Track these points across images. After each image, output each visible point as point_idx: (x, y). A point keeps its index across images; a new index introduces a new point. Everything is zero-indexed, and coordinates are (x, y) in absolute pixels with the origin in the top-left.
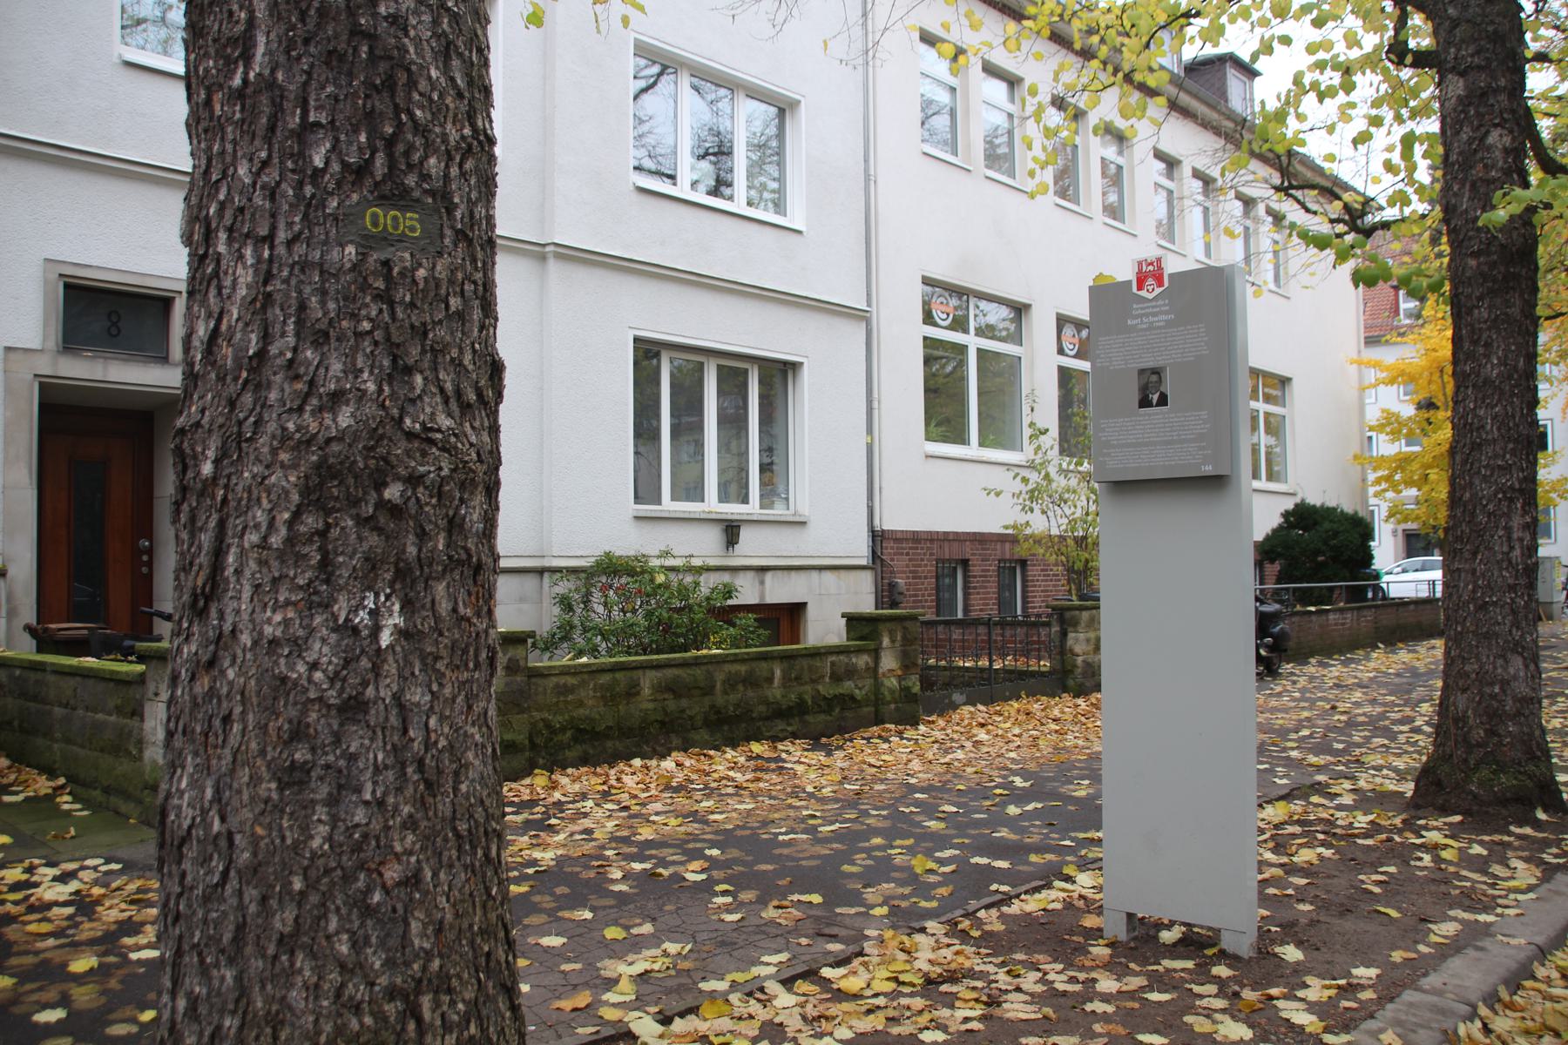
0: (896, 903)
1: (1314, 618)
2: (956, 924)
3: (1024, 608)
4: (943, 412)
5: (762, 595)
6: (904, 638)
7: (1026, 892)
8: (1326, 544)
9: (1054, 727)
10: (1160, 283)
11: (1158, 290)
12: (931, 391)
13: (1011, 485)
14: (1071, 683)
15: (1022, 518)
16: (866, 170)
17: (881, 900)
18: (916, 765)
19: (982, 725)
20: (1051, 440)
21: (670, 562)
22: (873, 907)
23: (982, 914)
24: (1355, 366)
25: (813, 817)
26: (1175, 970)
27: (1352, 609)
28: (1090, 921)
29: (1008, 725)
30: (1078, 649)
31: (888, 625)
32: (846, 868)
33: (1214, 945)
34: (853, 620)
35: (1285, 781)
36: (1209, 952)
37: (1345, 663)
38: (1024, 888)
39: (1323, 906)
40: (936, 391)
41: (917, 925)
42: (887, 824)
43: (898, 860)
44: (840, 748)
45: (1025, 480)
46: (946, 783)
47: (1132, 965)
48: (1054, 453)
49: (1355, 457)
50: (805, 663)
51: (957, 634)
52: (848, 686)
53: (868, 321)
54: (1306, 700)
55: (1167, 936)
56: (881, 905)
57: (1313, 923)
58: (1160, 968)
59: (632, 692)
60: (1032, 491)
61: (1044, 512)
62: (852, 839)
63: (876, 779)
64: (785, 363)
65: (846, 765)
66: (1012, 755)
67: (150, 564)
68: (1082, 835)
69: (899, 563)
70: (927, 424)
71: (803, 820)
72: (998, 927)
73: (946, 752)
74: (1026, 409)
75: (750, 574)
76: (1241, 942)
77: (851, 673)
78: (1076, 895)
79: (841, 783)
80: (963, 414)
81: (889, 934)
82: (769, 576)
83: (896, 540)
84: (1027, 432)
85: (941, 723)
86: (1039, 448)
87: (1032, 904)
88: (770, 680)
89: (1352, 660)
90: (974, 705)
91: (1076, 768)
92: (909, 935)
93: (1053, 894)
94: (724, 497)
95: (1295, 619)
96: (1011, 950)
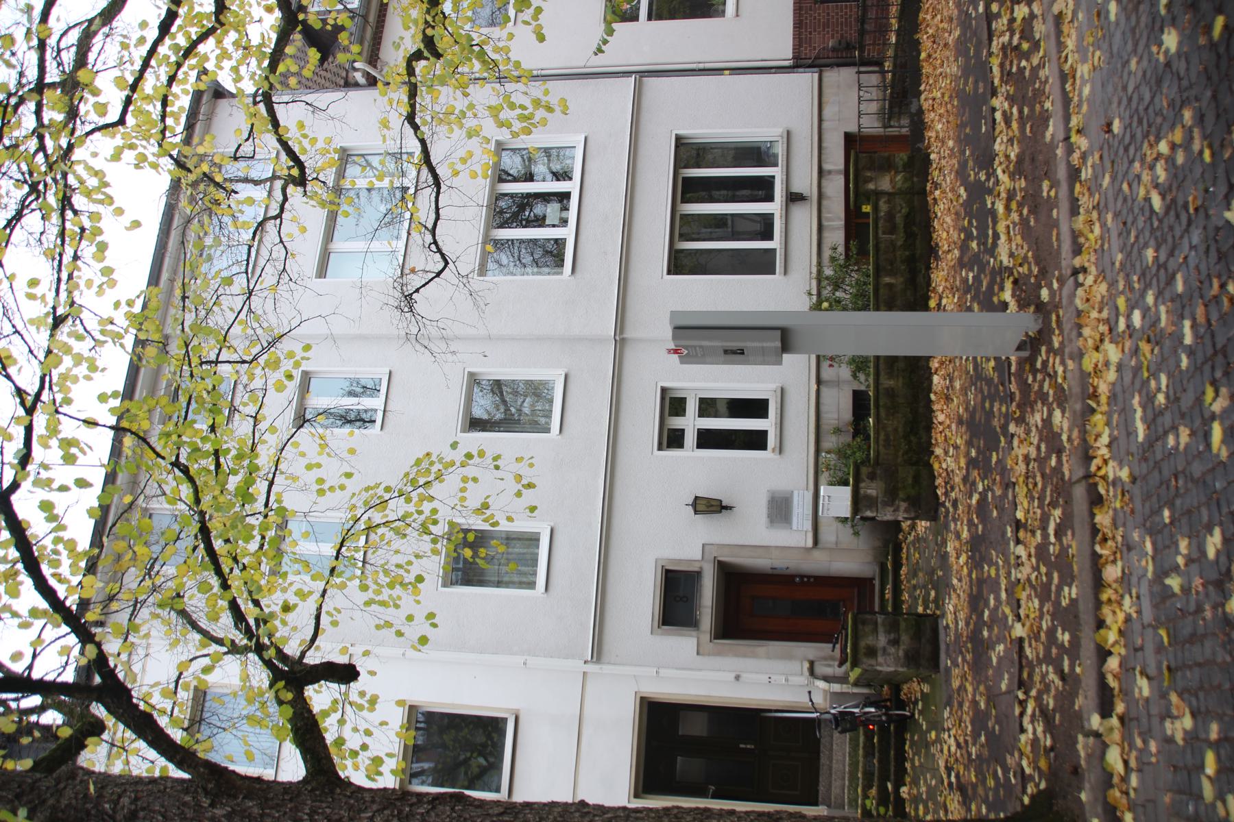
5: (838, 172)
21: (814, 292)
52: (899, 219)
59: (891, 393)
64: (677, 147)
67: (809, 577)
75: (824, 182)
82: (826, 167)
83: (800, 46)
88: (890, 286)
94: (769, 198)
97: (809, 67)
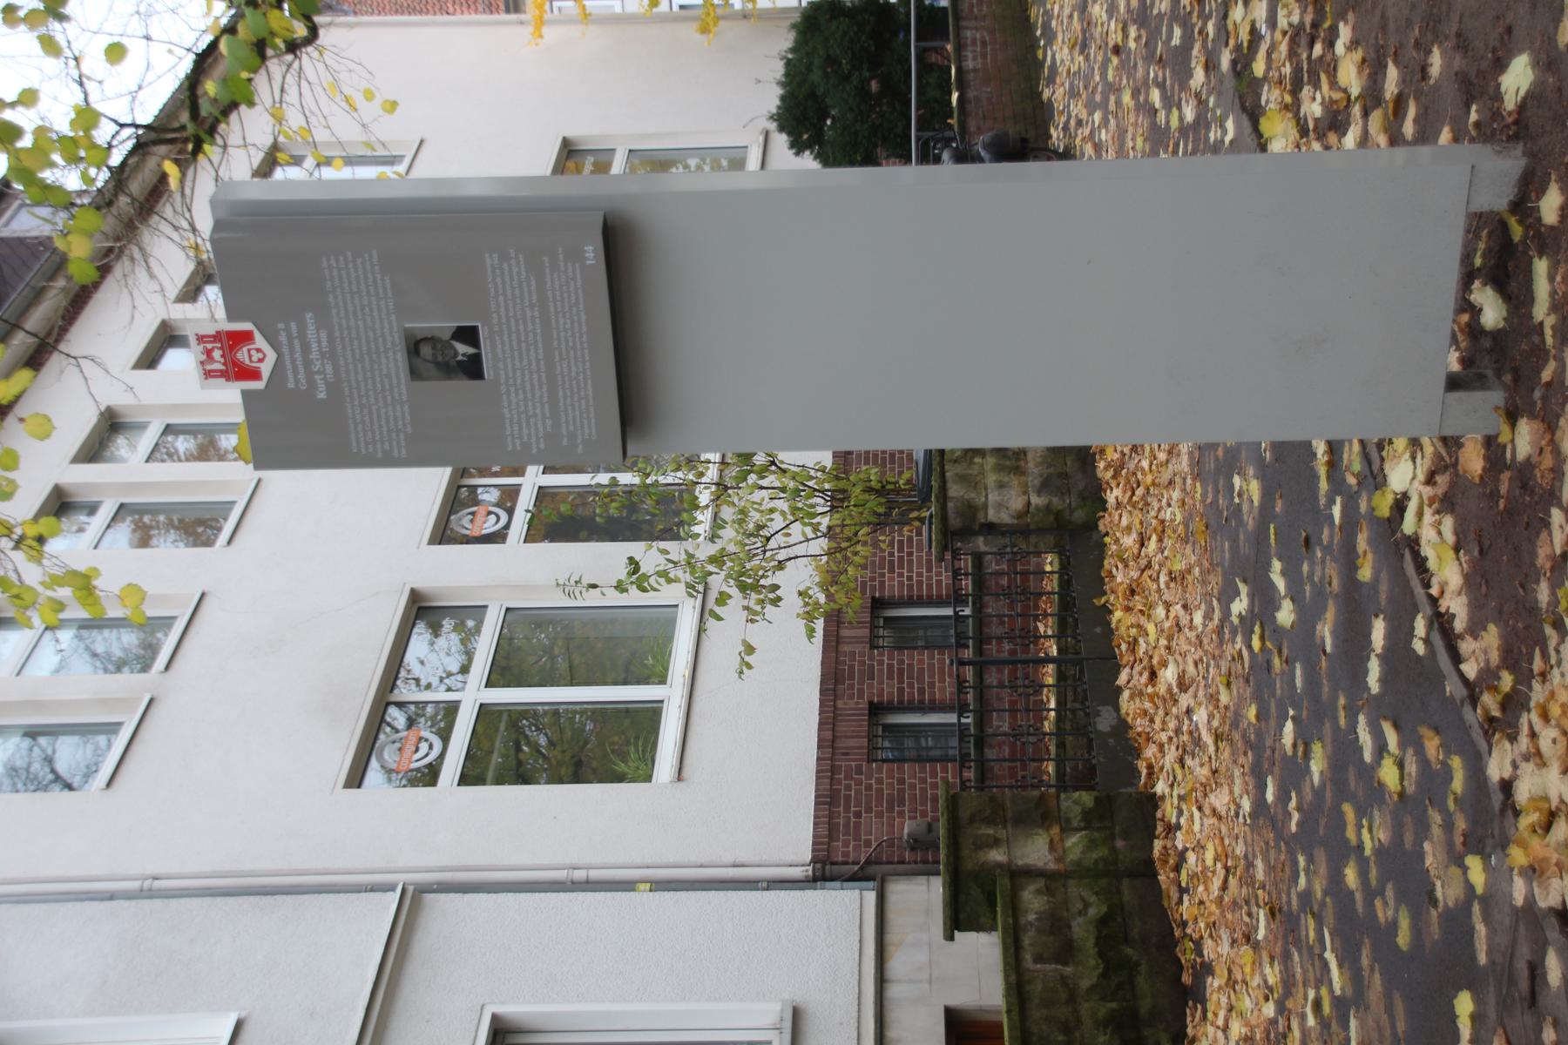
0: (1459, 840)
1: (971, 94)
2: (1491, 720)
3: (940, 603)
4: (607, 749)
6: (990, 821)
7: (1427, 585)
8: (846, 78)
9: (1152, 545)
10: (244, 337)
11: (260, 341)
12: (578, 772)
13: (732, 623)
14: (1079, 516)
15: (792, 603)
16: (129, 896)
17: (1455, 871)
18: (1219, 800)
19: (1153, 675)
20: (650, 555)
22: (1470, 887)
23: (1470, 669)
24: (545, 30)
25: (1317, 1005)
26: (1553, 293)
27: (958, 28)
28: (1473, 461)
29: (1151, 628)
30: (1017, 503)
31: (965, 852)
32: (1403, 939)
33: (1504, 226)
34: (958, 919)
35: (1230, 125)
36: (1517, 232)
37: (1050, 36)
38: (1419, 590)
39: (1432, 30)
40: (579, 764)
41: (1497, 799)
42: (1321, 856)
43: (1383, 835)
44: (1198, 945)
45: (723, 599)
46: (1247, 743)
47: (1546, 375)
48: (675, 549)
49: (705, 30)
50: (1036, 1014)
51: (1001, 723)
52: (1082, 930)
53: (423, 889)
54: (1106, 100)
55: (1492, 312)
56: (1465, 869)
57: (1462, 44)
58: (1550, 321)
60: (743, 588)
61: (781, 565)
62: (1354, 930)
63: (1248, 879)
65: (1225, 935)
66: (1198, 618)
68: (1324, 485)
69: (875, 830)
70: (620, 778)
71: (1324, 1023)
72: (1492, 637)
73: (1197, 741)
74: (592, 599)
76: (1493, 175)
77: (1056, 923)
78: (1428, 491)
79: (1256, 947)
80: (602, 713)
81: (1518, 856)
83: (832, 836)
84: (634, 597)
85: (1150, 751)
86: (663, 574)
87: (1448, 573)
89: (1046, 26)
90: (1119, 690)
91: (1215, 502)
92: (1517, 814)
93: (1428, 534)
95: (972, 125)
96: (1533, 610)
97: (854, 878)
